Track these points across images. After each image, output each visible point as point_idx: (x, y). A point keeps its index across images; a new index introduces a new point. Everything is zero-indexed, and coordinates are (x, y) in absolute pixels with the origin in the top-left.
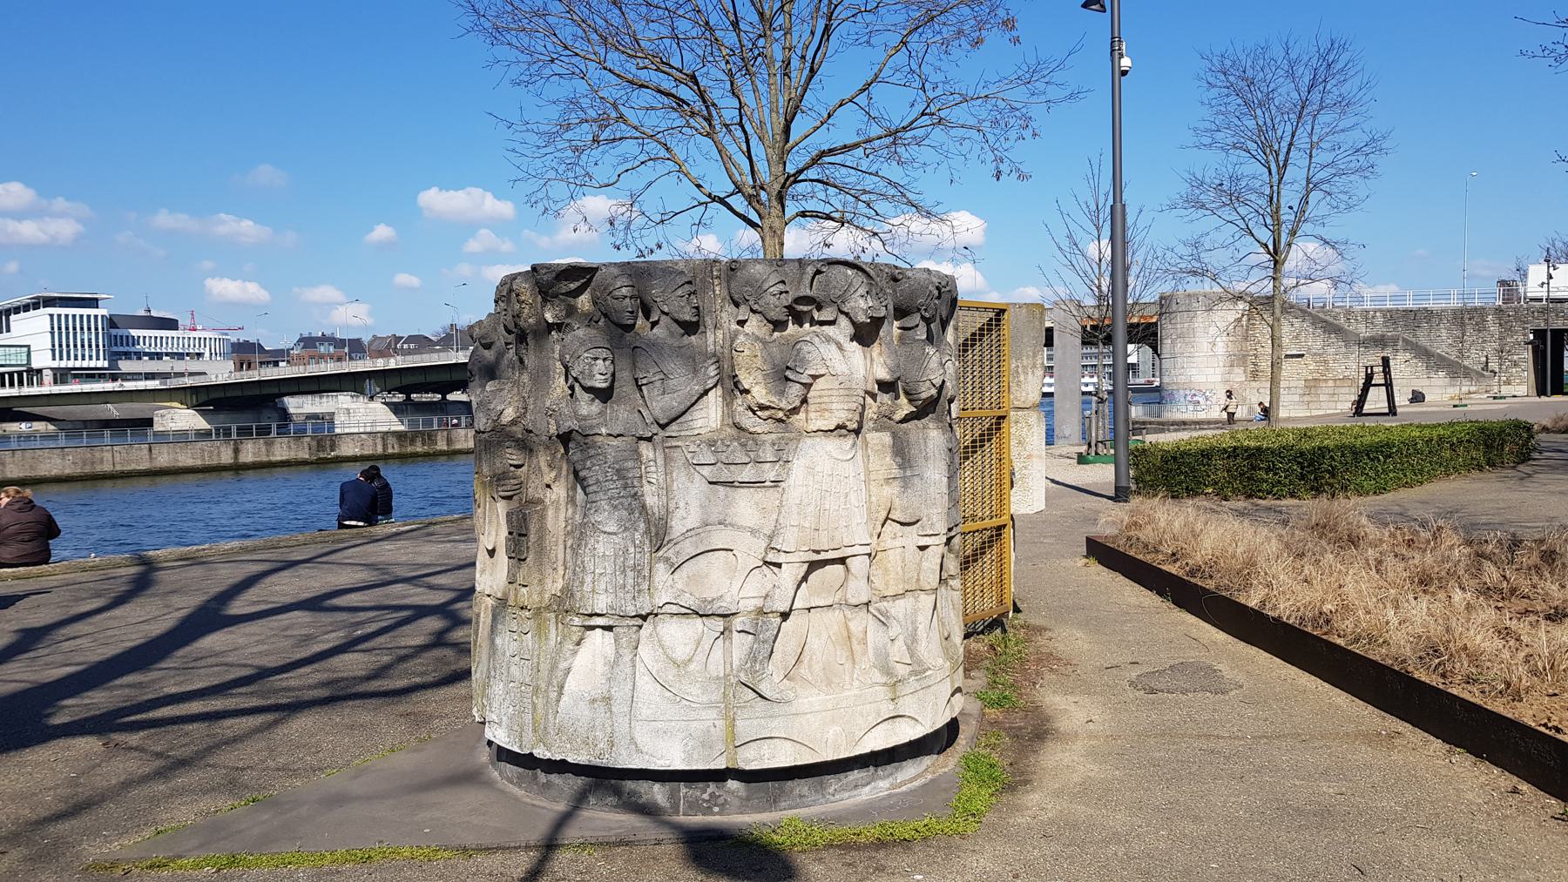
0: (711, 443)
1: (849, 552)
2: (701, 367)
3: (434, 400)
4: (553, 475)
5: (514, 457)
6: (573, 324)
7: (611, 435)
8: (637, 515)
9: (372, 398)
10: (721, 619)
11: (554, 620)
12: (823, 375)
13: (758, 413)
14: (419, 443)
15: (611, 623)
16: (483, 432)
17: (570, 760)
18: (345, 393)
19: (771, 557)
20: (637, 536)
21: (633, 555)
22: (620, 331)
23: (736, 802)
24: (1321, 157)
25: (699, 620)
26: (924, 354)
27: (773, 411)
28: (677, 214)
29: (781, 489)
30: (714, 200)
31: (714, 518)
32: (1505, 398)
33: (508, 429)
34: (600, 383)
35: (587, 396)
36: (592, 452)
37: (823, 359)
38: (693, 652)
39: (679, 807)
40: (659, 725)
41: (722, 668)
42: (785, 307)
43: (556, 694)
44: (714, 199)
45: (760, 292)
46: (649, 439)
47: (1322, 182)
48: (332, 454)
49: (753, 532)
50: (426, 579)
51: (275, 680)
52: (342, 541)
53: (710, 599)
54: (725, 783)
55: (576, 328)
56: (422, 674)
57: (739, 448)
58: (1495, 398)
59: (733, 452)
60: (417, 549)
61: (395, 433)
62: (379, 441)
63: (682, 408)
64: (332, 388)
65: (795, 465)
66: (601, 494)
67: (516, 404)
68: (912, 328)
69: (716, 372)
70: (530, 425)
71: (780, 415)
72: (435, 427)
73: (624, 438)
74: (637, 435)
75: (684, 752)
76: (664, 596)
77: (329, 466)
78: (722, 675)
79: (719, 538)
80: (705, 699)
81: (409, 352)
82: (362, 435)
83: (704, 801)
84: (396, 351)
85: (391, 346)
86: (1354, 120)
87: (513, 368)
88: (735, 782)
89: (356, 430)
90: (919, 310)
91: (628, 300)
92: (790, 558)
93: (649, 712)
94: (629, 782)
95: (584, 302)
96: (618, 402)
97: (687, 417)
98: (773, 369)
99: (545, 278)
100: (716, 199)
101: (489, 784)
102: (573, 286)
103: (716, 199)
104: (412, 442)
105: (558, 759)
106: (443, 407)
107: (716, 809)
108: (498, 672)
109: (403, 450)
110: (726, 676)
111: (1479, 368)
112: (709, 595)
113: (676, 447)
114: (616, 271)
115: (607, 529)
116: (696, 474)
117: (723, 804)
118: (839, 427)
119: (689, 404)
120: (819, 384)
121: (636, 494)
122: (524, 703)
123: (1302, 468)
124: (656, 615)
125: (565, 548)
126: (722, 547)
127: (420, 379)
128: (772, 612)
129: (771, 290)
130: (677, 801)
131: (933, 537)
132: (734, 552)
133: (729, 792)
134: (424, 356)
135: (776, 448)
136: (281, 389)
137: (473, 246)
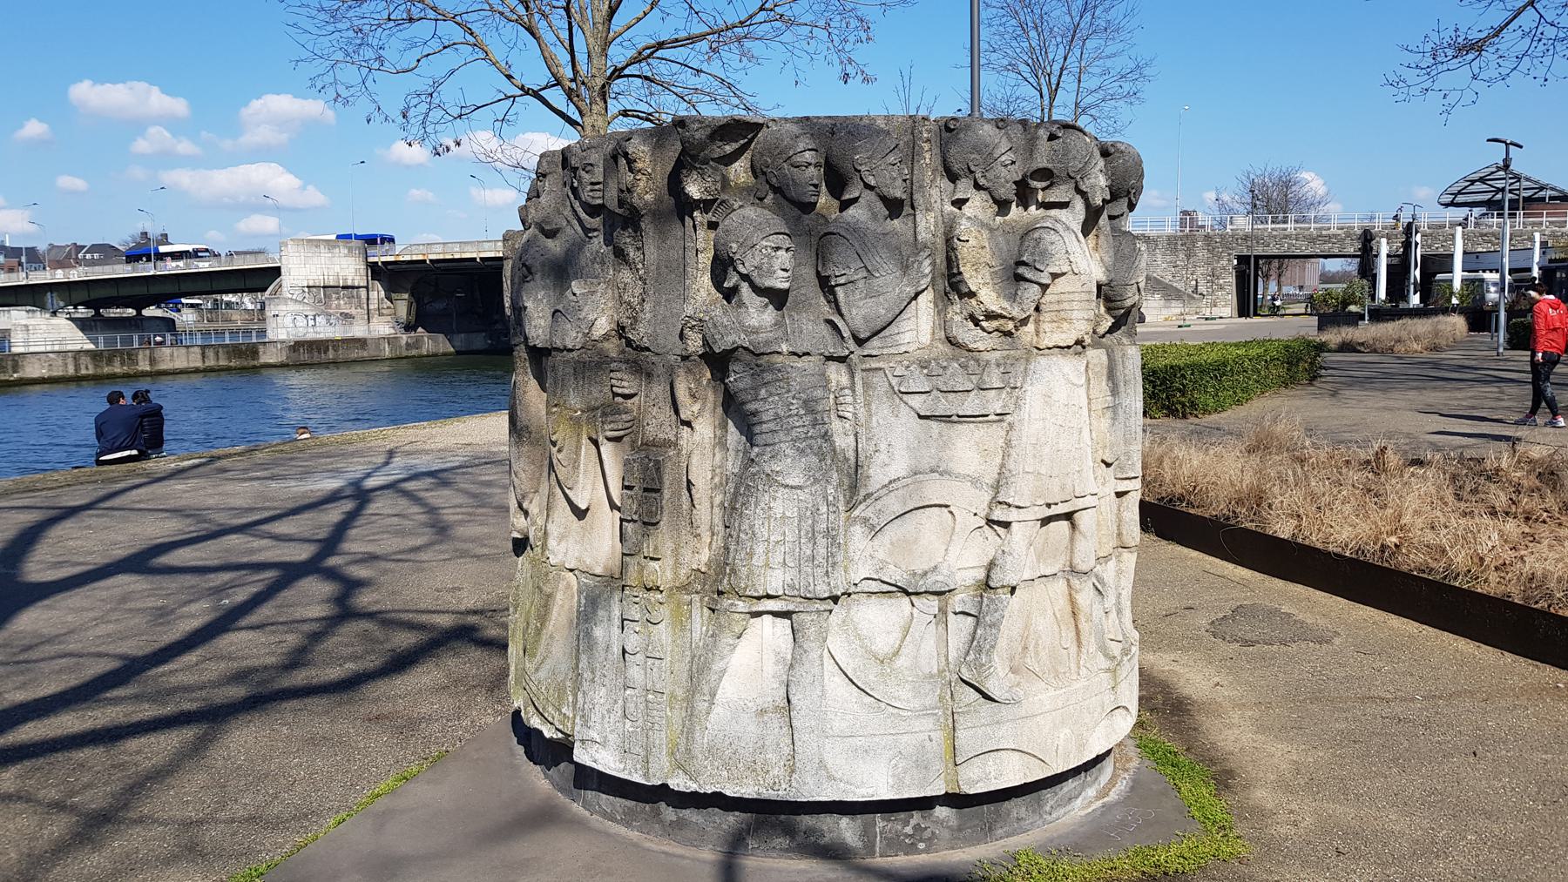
0: (924, 365)
1: (1080, 504)
2: (913, 262)
3: (124, 315)
4: (696, 408)
5: (625, 384)
6: (732, 202)
7: (794, 354)
8: (829, 462)
9: (54, 313)
10: (936, 597)
11: (699, 604)
12: (1064, 274)
13: (983, 323)
14: (117, 363)
15: (791, 607)
16: (570, 350)
17: (728, 793)
18: (19, 308)
19: (999, 514)
20: (830, 490)
21: (825, 516)
22: (797, 212)
23: (946, 834)
24: (1089, 83)
25: (906, 600)
26: (1135, 250)
27: (1002, 321)
28: (479, 108)
29: (1005, 424)
30: (527, 93)
31: (926, 464)
32: (1215, 319)
33: (600, 345)
34: (779, 282)
35: (760, 301)
36: (768, 377)
37: (1067, 252)
38: (898, 642)
39: (874, 846)
40: (858, 742)
41: (934, 662)
42: (1015, 183)
43: (706, 704)
44: (526, 91)
45: (990, 160)
46: (842, 360)
47: (1090, 107)
48: (15, 375)
49: (975, 482)
50: (265, 527)
51: (163, 674)
52: (113, 481)
53: (920, 572)
54: (931, 812)
55: (736, 206)
56: (354, 658)
57: (960, 370)
58: (1207, 319)
59: (953, 375)
60: (220, 489)
61: (88, 351)
62: (70, 361)
63: (890, 316)
64: (8, 301)
65: (1029, 393)
66: (781, 434)
67: (610, 313)
68: (1118, 217)
70: (645, 340)
71: (1010, 326)
72: (136, 345)
73: (810, 358)
74: (827, 354)
75: (894, 776)
77: (12, 389)
78: (935, 671)
79: (935, 490)
80: (916, 704)
81: (92, 263)
82: (50, 355)
83: (907, 836)
84: (78, 262)
85: (70, 255)
86: (1120, 46)
87: (603, 263)
88: (944, 808)
89: (42, 349)
91: (812, 168)
92: (1023, 515)
93: (844, 725)
94: (807, 817)
95: (739, 171)
96: (796, 308)
97: (892, 329)
98: (1001, 265)
99: (698, 135)
100: (530, 92)
101: (577, 824)
102: (729, 149)
103: (530, 92)
104: (110, 362)
105: (709, 792)
106: (138, 323)
107: (922, 846)
108: (598, 674)
109: (99, 371)
110: (940, 672)
111: (1190, 291)
112: (919, 567)
113: (876, 369)
114: (795, 129)
115: (790, 482)
116: (903, 405)
117: (929, 839)
119: (897, 312)
121: (826, 433)
122: (653, 717)
123: (1154, 387)
124: (849, 595)
125: (712, 507)
126: (937, 502)
127: (112, 292)
128: (1003, 587)
129: (1003, 158)
130: (871, 839)
131: (1133, 480)
132: (952, 509)
133: (939, 822)
134: (115, 267)
135: (1002, 370)
136: (247, 282)
137: (141, 146)
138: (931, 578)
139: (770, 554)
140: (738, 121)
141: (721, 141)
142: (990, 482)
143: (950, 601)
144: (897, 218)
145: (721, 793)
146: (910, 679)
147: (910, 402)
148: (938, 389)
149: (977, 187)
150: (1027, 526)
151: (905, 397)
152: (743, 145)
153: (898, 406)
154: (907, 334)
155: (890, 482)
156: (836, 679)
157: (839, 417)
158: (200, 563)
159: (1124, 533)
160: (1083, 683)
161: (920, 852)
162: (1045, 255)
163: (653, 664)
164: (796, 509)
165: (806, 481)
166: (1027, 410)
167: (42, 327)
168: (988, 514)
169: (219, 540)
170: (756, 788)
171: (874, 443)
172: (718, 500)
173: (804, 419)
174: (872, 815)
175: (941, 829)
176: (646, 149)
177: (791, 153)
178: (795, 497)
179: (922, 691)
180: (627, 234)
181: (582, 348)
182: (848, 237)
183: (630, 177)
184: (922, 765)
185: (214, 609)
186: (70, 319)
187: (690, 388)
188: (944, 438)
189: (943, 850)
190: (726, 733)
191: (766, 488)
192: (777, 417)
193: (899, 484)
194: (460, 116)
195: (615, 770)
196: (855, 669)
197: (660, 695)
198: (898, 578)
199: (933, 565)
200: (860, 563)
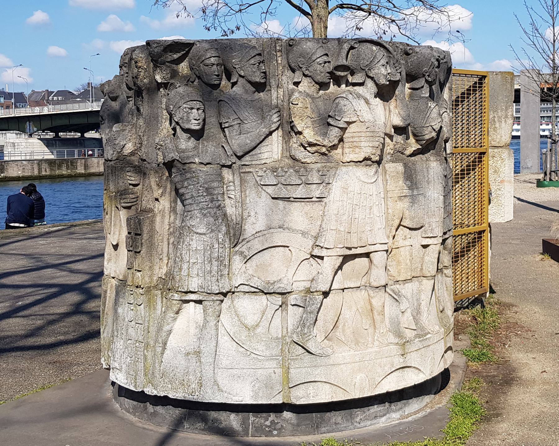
0: (274, 170)
1: (372, 248)
2: (267, 116)
3: (76, 137)
4: (160, 191)
5: (133, 179)
7: (202, 163)
8: (220, 221)
9: (31, 135)
10: (280, 296)
11: (160, 296)
12: (355, 122)
13: (308, 148)
14: (64, 168)
15: (201, 298)
16: (111, 161)
17: (170, 396)
18: (12, 132)
19: (316, 252)
20: (220, 236)
21: (217, 249)
22: (209, 89)
23: (290, 427)
25: (264, 297)
26: (427, 107)
27: (318, 147)
28: (251, 5)
31: (275, 224)
33: (128, 158)
34: (194, 126)
35: (185, 136)
36: (188, 175)
37: (355, 110)
39: (248, 430)
40: (234, 372)
42: (328, 73)
43: (161, 348)
45: (310, 61)
46: (230, 167)
48: (2, 175)
49: (304, 234)
53: (272, 282)
54: (281, 414)
55: (177, 86)
56: (65, 333)
57: (294, 173)
59: (290, 176)
60: (63, 244)
62: (36, 166)
63: (254, 144)
65: (334, 186)
66: (195, 205)
67: (134, 141)
69: (278, 119)
70: (144, 155)
71: (324, 150)
73: (211, 166)
74: (221, 164)
75: (253, 391)
76: (239, 279)
78: (280, 336)
79: (279, 238)
80: (268, 353)
81: (58, 103)
82: (24, 162)
83: (267, 426)
87: (132, 115)
89: (19, 158)
90: (424, 76)
91: (215, 67)
92: (329, 252)
93: (228, 362)
94: (213, 412)
95: (183, 68)
96: (207, 140)
97: (257, 151)
99: (156, 50)
101: (112, 413)
102: (176, 56)
104: (60, 167)
105: (162, 395)
106: (82, 142)
107: (275, 432)
109: (53, 173)
112: (272, 279)
113: (248, 172)
114: (206, 46)
115: (199, 231)
116: (263, 192)
117: (280, 429)
118: (366, 159)
119: (258, 142)
120: (352, 128)
121: (219, 206)
124: (233, 293)
125: (169, 244)
127: (65, 122)
128: (317, 291)
129: (318, 60)
132: (290, 248)
133: (285, 420)
134: (68, 105)
135: (320, 173)
137: (104, 27)
138: (277, 286)
139: (190, 269)
140: (177, 42)
141: (171, 52)
142: (314, 235)
143: (289, 299)
144: (263, 92)
145: (167, 396)
146: (264, 339)
147: (266, 190)
148: (282, 184)
149: (305, 75)
150: (332, 259)
151: (264, 187)
152: (183, 55)
153: (260, 192)
154: (266, 154)
155: (256, 233)
156: (225, 338)
157: (229, 197)
158: (21, 283)
159: (424, 268)
160: (376, 349)
161: (274, 436)
162: (341, 112)
163: (139, 327)
164: (202, 246)
165: (207, 231)
166: (333, 195)
167: (23, 144)
168: (311, 252)
169: (40, 271)
170: (184, 394)
171: (248, 211)
172: (171, 241)
173: (206, 198)
174: (247, 414)
175: (287, 424)
176: (143, 56)
177: (203, 59)
178: (202, 239)
179: (271, 346)
180: (139, 99)
181: (117, 159)
182: (229, 103)
183: (136, 70)
184: (268, 386)
185: (10, 306)
186: (40, 139)
187: (156, 181)
188: (287, 210)
189: (288, 436)
190: (171, 364)
191: (188, 234)
192: (192, 196)
193: (260, 234)
194: (240, 10)
195: (123, 383)
196: (234, 333)
197: (141, 343)
198: (259, 284)
199: (279, 278)
200: (238, 276)
